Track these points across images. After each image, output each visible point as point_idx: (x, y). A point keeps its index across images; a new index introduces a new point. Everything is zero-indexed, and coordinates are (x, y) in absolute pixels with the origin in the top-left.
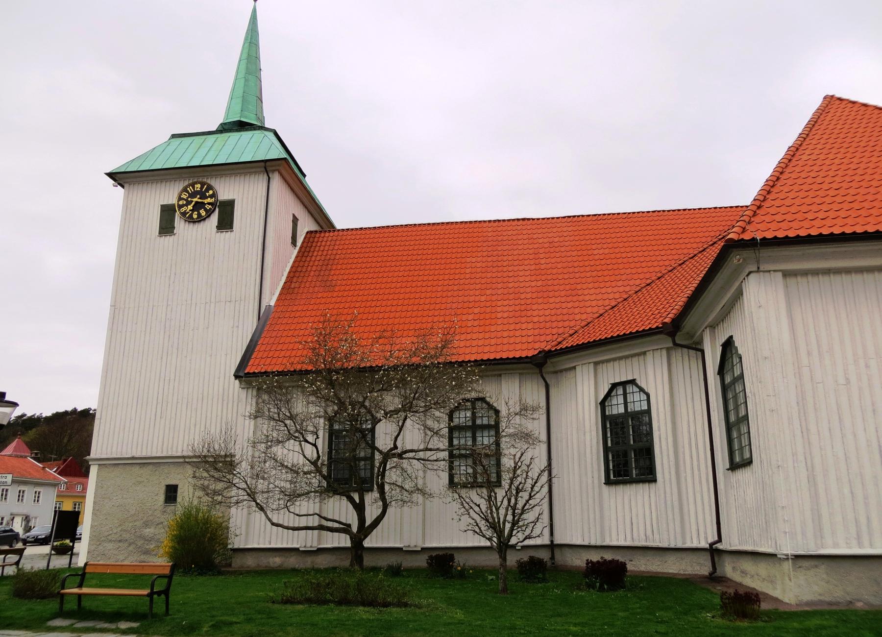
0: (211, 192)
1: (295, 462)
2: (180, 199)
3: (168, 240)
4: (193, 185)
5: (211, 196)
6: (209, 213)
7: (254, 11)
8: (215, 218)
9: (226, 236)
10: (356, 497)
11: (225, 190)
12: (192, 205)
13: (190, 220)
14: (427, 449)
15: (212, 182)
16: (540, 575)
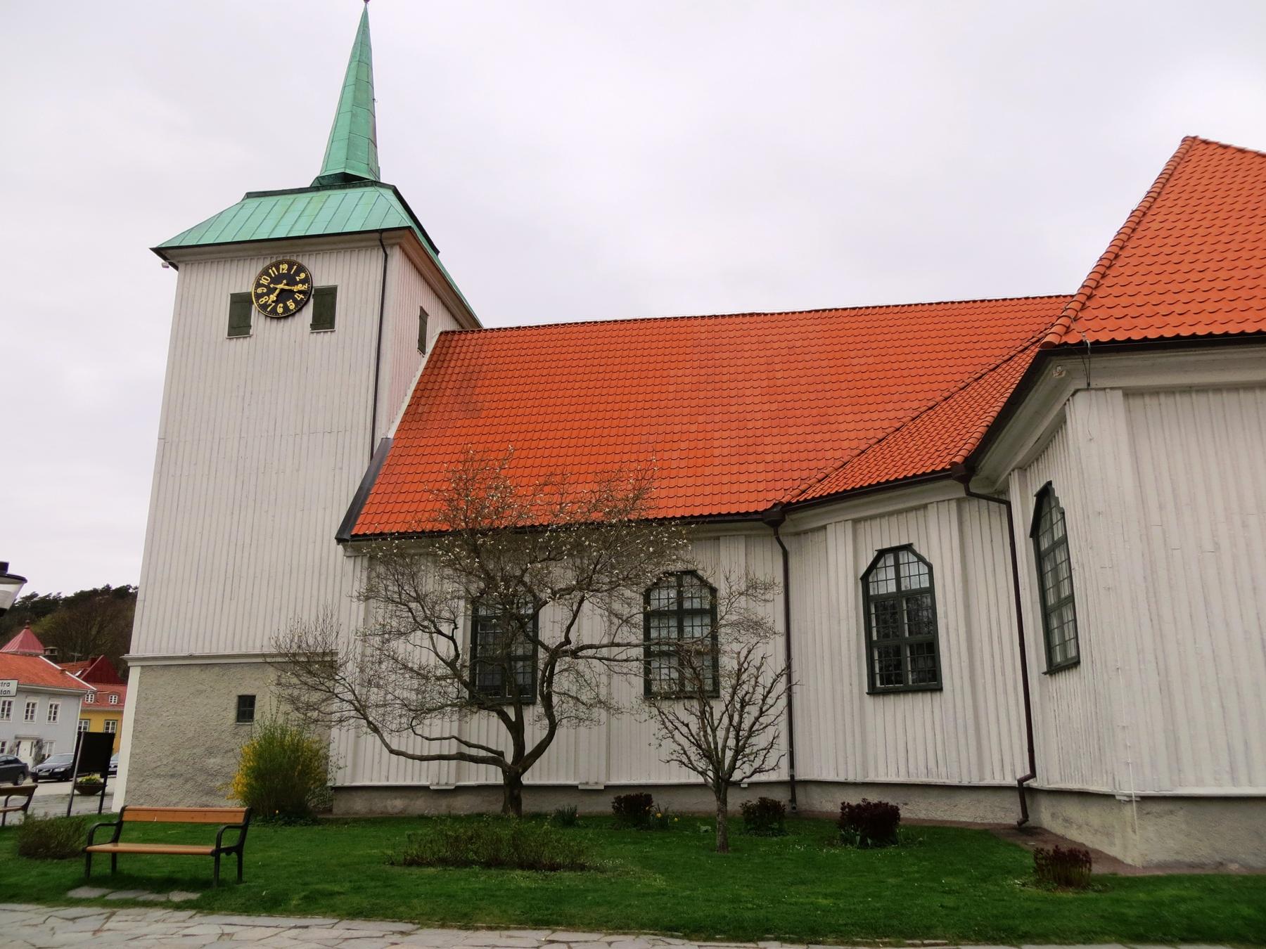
0: (303, 276)
2: (258, 285)
3: (240, 344)
4: (277, 266)
5: (303, 282)
6: (300, 306)
7: (365, 16)
8: (308, 312)
9: (324, 338)
10: (511, 713)
11: (323, 272)
12: (275, 294)
13: (273, 316)
14: (613, 644)
15: (305, 261)
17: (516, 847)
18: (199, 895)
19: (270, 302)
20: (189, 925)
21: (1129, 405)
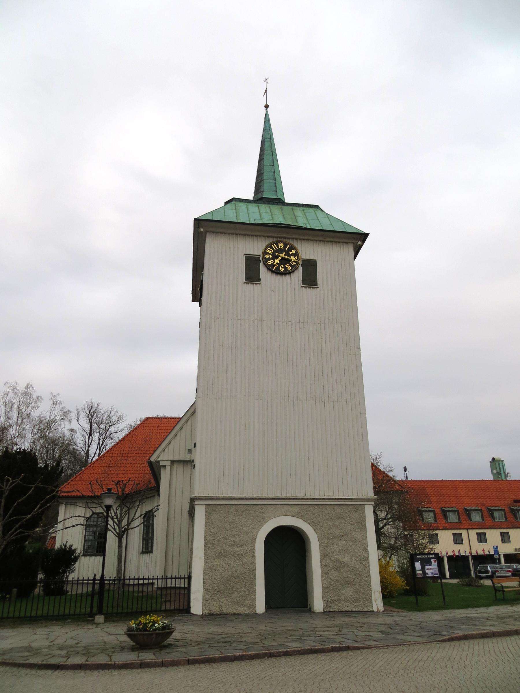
0: (294, 252)
3: (252, 288)
5: (295, 255)
6: (294, 268)
8: (298, 275)
9: (309, 292)
13: (277, 272)
15: (295, 244)
19: (275, 263)
20: (401, 640)
21: (282, 211)
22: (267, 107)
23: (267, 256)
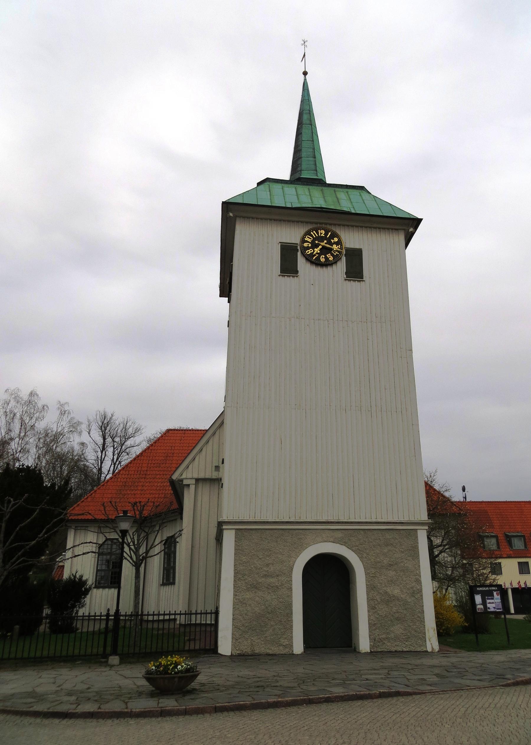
0: (336, 240)
1: (94, 548)
3: (289, 281)
5: (337, 243)
6: (337, 259)
9: (354, 285)
12: (319, 249)
13: (317, 263)
16: (189, 667)
17: (447, 576)
18: (524, 616)
22: (305, 73)
23: (306, 245)
